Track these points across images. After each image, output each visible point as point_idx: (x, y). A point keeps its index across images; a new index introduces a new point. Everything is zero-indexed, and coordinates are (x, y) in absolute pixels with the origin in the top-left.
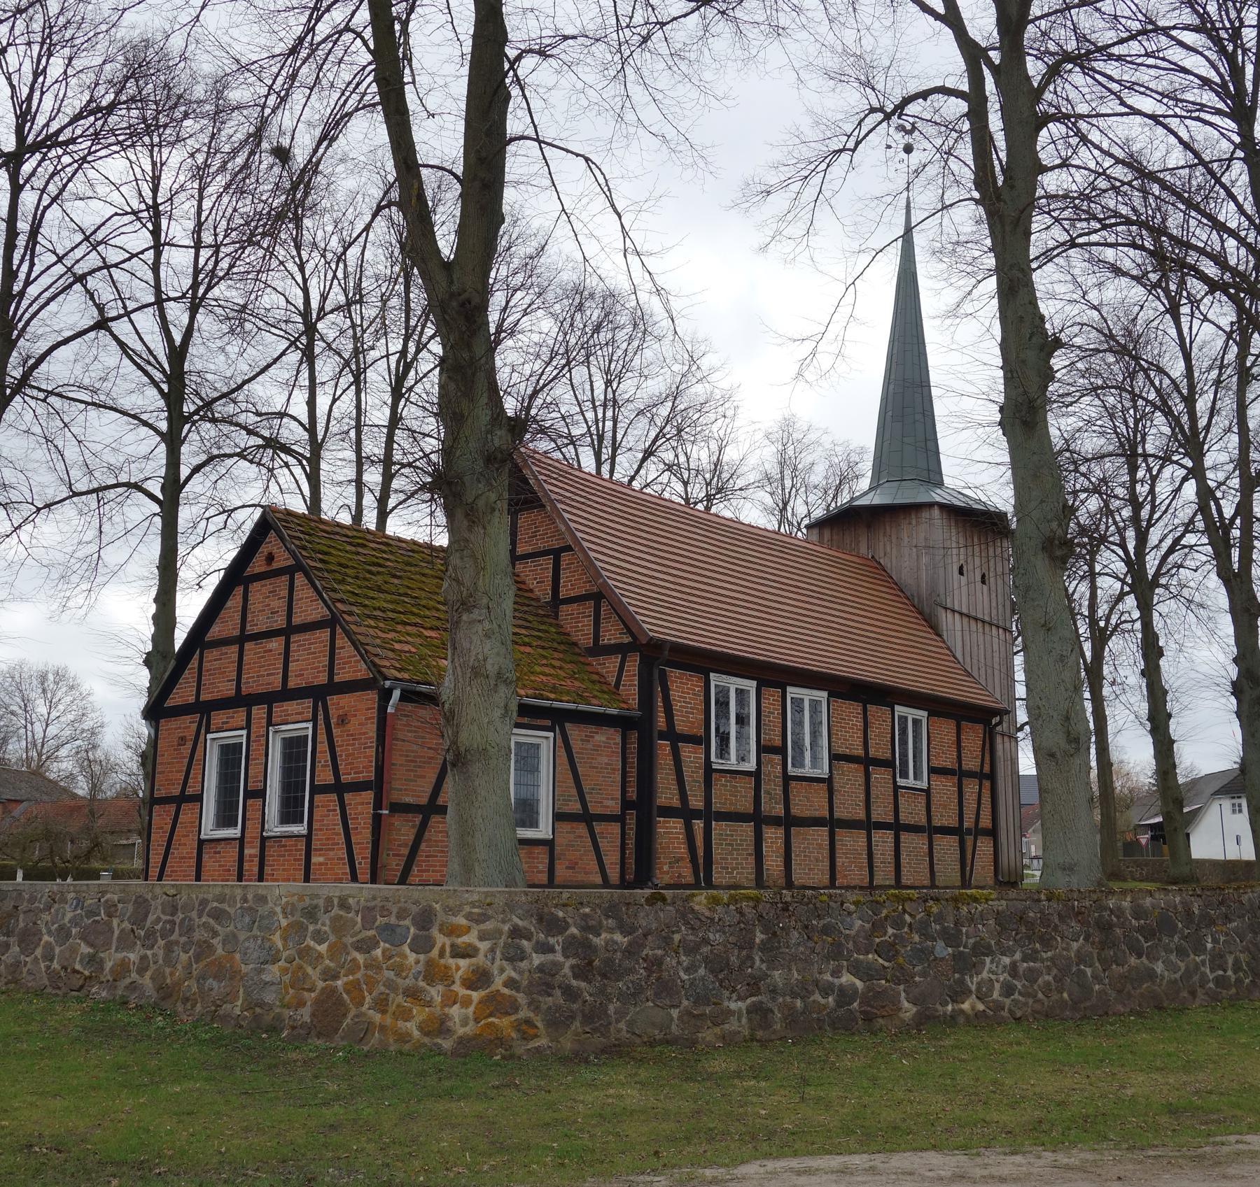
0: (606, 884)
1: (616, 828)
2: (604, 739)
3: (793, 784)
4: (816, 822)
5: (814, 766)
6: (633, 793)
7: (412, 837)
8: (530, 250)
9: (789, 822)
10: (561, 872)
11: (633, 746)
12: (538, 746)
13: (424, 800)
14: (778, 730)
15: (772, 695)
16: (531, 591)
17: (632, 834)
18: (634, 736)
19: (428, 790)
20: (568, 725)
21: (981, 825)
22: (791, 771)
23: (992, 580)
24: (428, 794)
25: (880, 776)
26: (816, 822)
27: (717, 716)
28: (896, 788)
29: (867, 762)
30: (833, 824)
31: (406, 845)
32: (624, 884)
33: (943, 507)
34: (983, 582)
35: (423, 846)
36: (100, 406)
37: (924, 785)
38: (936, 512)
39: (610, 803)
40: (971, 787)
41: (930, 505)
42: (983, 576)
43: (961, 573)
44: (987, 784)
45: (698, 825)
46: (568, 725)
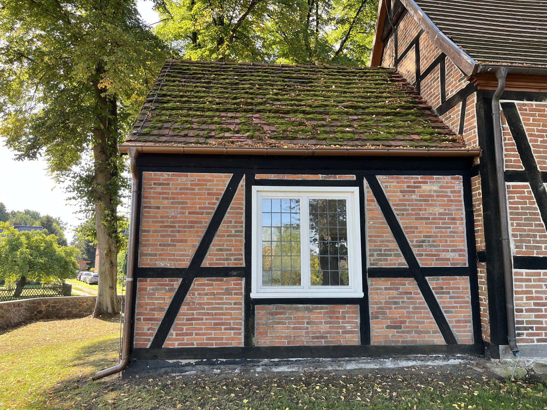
0: (451, 346)
1: (464, 282)
2: (435, 188)
3: (260, 312)
6: (481, 244)
7: (169, 301)
8: (167, 7)
10: (380, 333)
11: (477, 193)
12: (342, 203)
13: (185, 263)
16: (423, 9)
17: (483, 288)
18: (477, 182)
19: (191, 253)
20: (381, 179)
24: (190, 258)
31: (161, 309)
32: (480, 349)
35: (183, 309)
39: (456, 255)
46: (381, 179)
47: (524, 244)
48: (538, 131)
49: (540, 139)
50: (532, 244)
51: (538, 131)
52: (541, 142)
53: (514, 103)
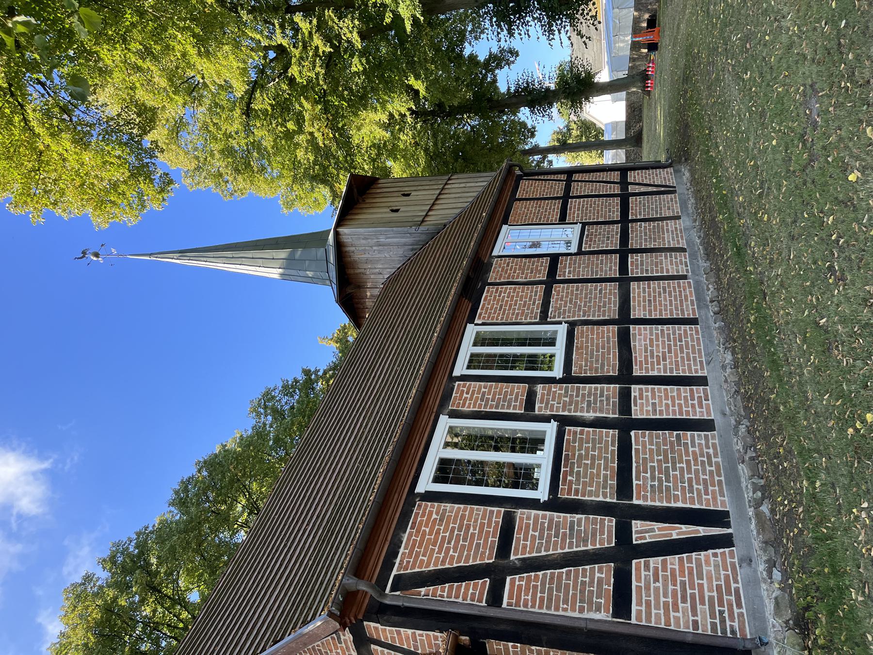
3: (563, 495)
4: (624, 341)
5: (551, 342)
9: (625, 376)
14: (505, 387)
15: (466, 396)
21: (637, 525)
22: (574, 249)
23: (406, 189)
25: (565, 271)
26: (624, 341)
27: (478, 483)
28: (568, 378)
29: (551, 280)
30: (624, 320)
33: (339, 224)
34: (408, 195)
36: (330, 531)
37: (550, 429)
38: (340, 230)
40: (577, 189)
41: (337, 234)
42: (404, 195)
43: (397, 211)
44: (576, 177)
45: (644, 532)
47: (595, 599)
48: (439, 552)
49: (451, 553)
50: (595, 589)
51: (439, 552)
52: (455, 552)
53: (395, 576)
